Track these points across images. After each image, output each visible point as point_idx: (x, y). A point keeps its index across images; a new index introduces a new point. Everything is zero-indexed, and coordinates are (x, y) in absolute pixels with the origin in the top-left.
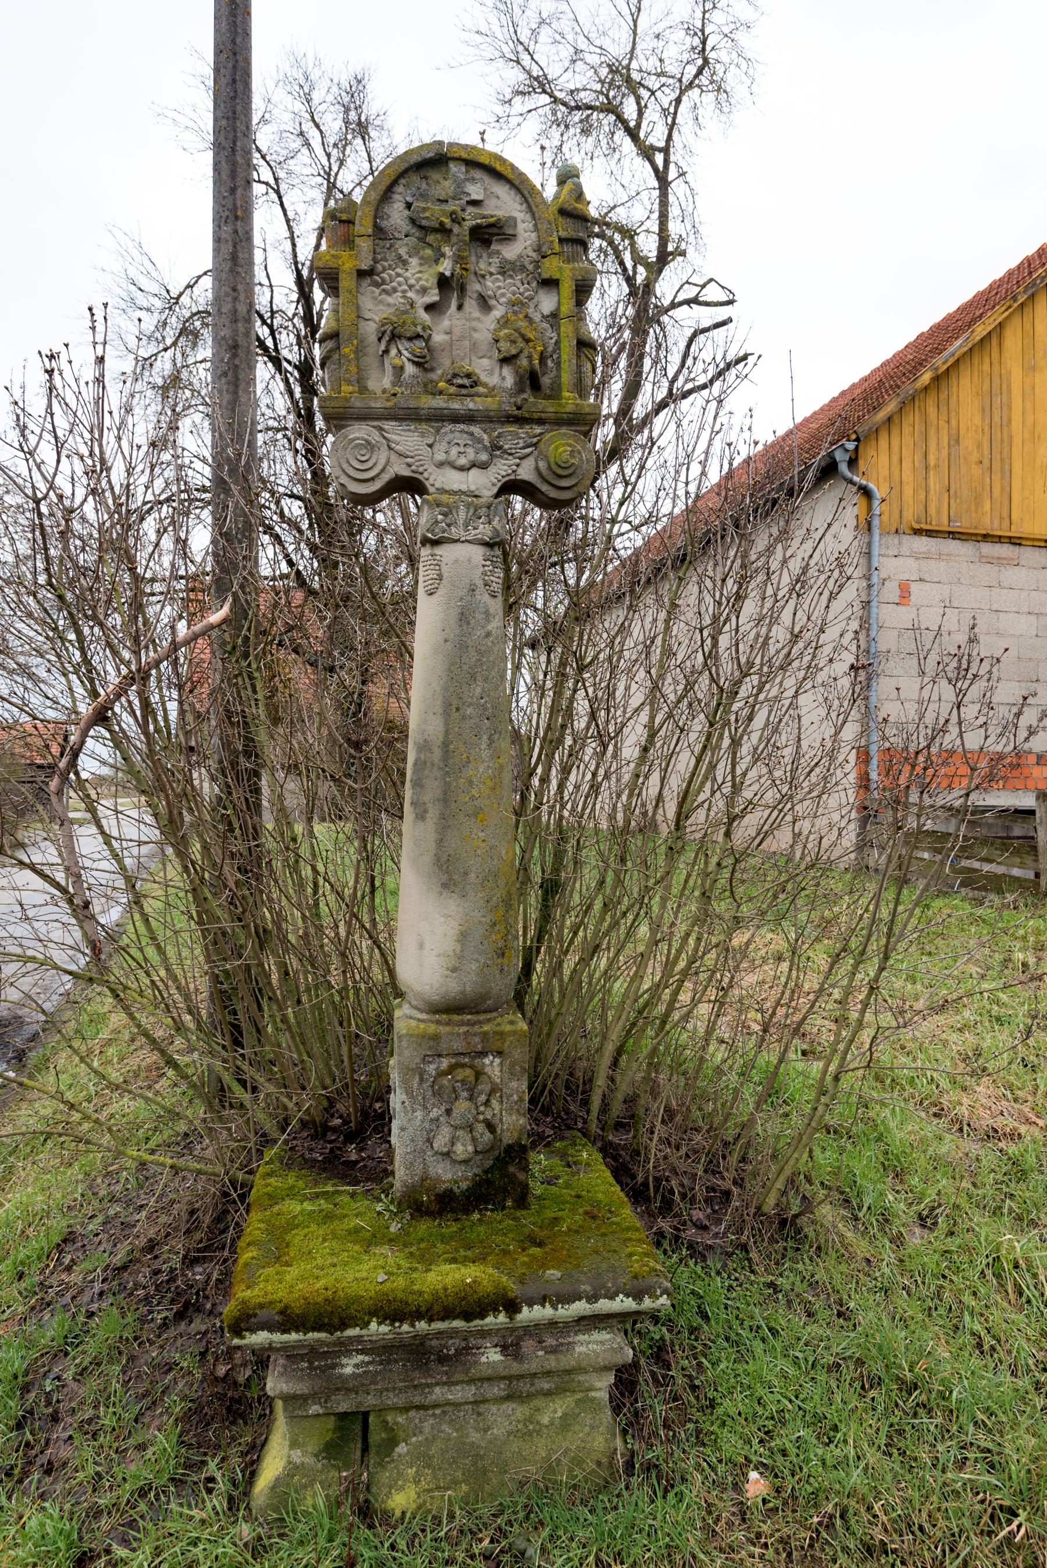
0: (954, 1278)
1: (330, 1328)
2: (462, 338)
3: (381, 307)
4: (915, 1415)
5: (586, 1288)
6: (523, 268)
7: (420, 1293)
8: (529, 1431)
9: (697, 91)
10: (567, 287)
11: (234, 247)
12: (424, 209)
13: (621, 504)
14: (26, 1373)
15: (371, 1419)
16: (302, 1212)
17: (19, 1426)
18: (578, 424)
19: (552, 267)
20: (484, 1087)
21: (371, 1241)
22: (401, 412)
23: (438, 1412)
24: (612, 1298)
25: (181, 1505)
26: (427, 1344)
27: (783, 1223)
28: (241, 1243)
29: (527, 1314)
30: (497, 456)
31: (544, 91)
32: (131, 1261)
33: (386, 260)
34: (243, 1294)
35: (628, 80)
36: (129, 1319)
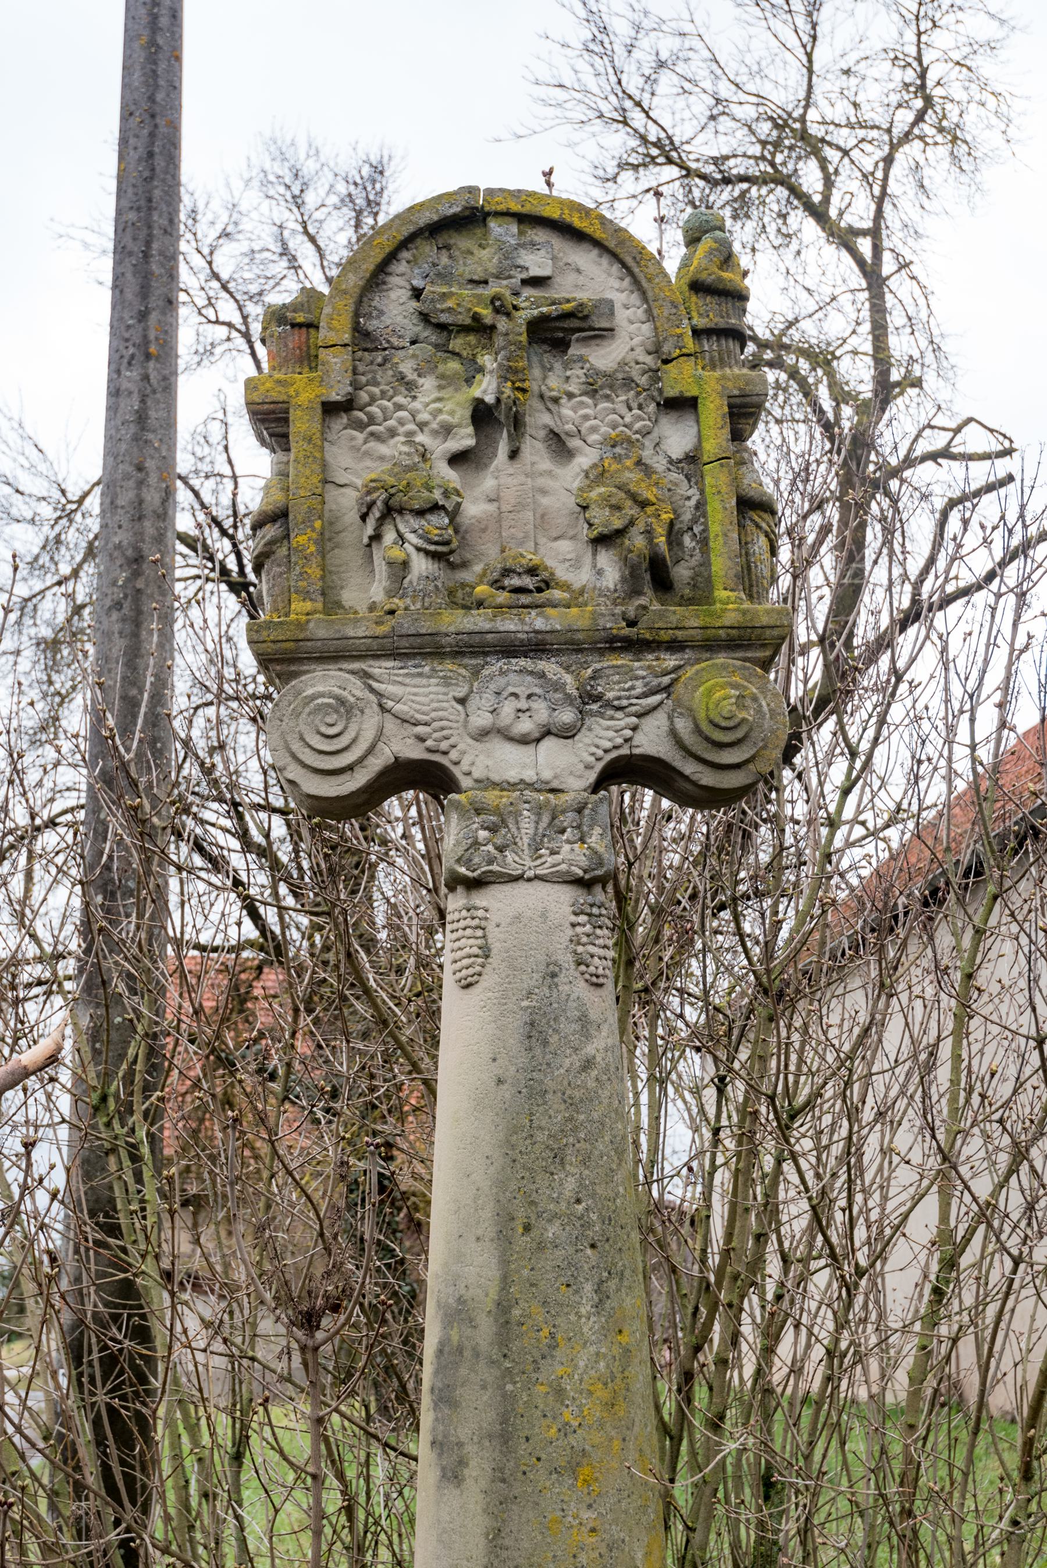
2: (520, 506)
3: (368, 463)
6: (629, 382)
9: (917, 144)
10: (713, 410)
11: (143, 401)
12: (444, 296)
13: (846, 792)
18: (748, 647)
19: (680, 379)
22: (404, 643)
30: (592, 714)
31: (670, 161)
33: (376, 384)
35: (804, 135)
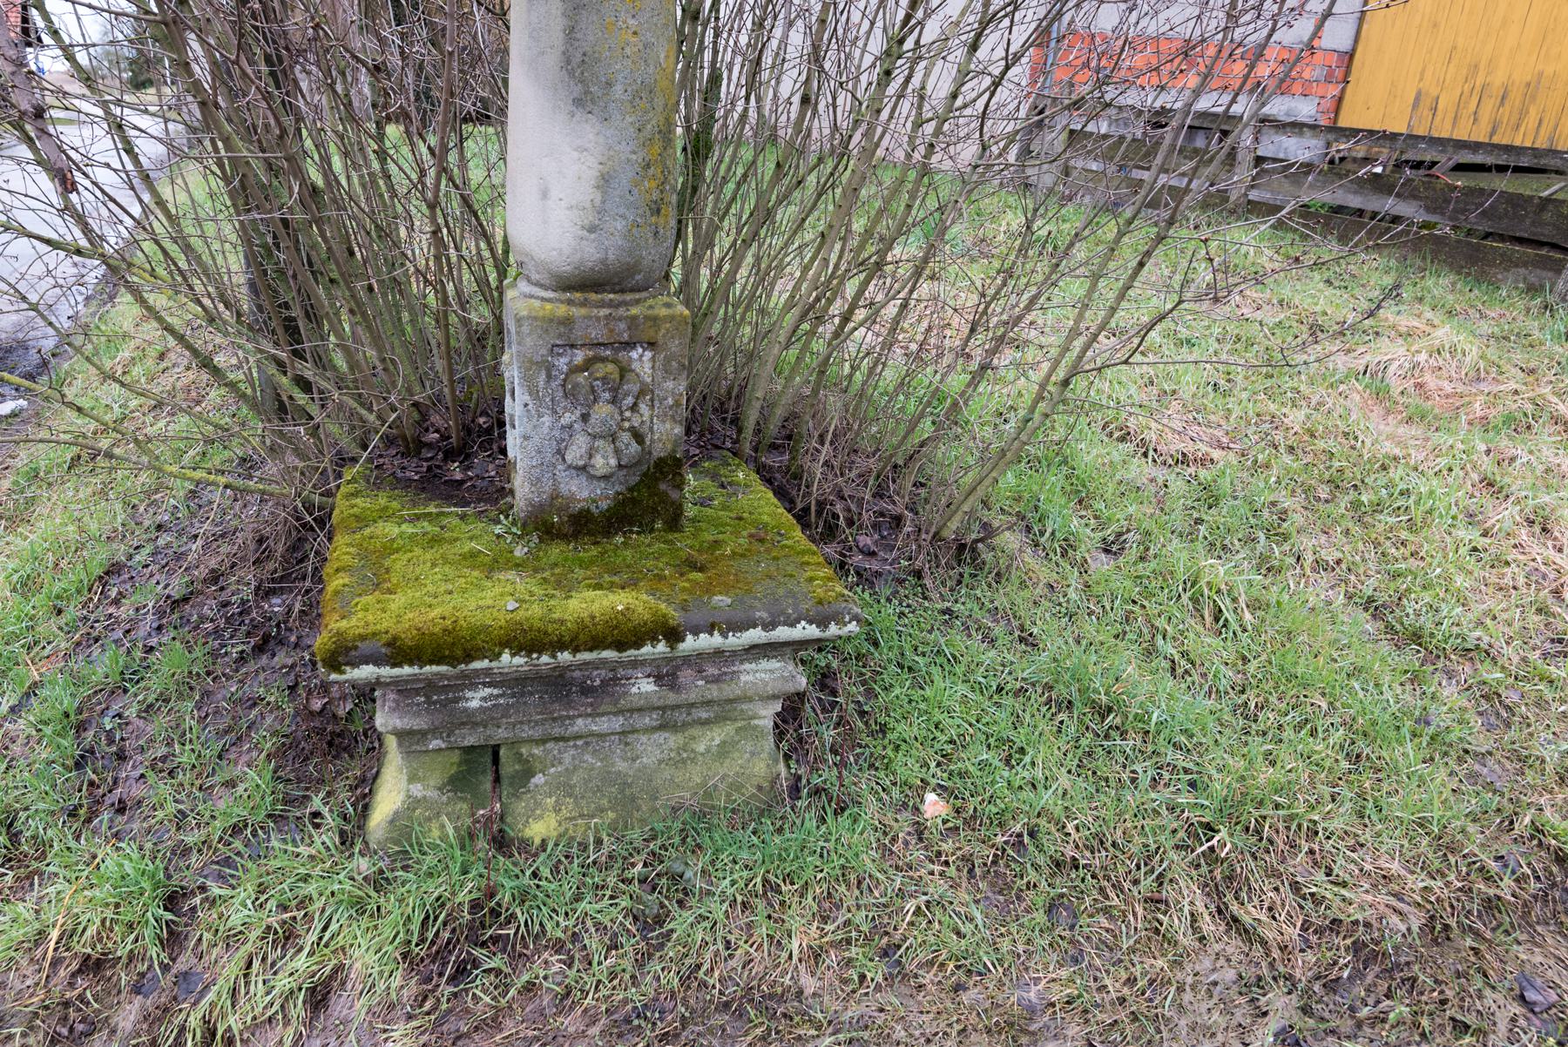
0: (1146, 603)
1: (452, 661)
4: (1107, 737)
5: (762, 614)
7: (562, 622)
8: (682, 759)
14: (79, 711)
15: (502, 752)
16: (401, 535)
17: (78, 765)
20: (632, 387)
21: (492, 567)
23: (579, 743)
24: (792, 625)
25: (284, 841)
26: (566, 676)
27: (962, 547)
28: (328, 569)
29: (690, 644)
32: (192, 593)
34: (336, 624)
36: (198, 652)
